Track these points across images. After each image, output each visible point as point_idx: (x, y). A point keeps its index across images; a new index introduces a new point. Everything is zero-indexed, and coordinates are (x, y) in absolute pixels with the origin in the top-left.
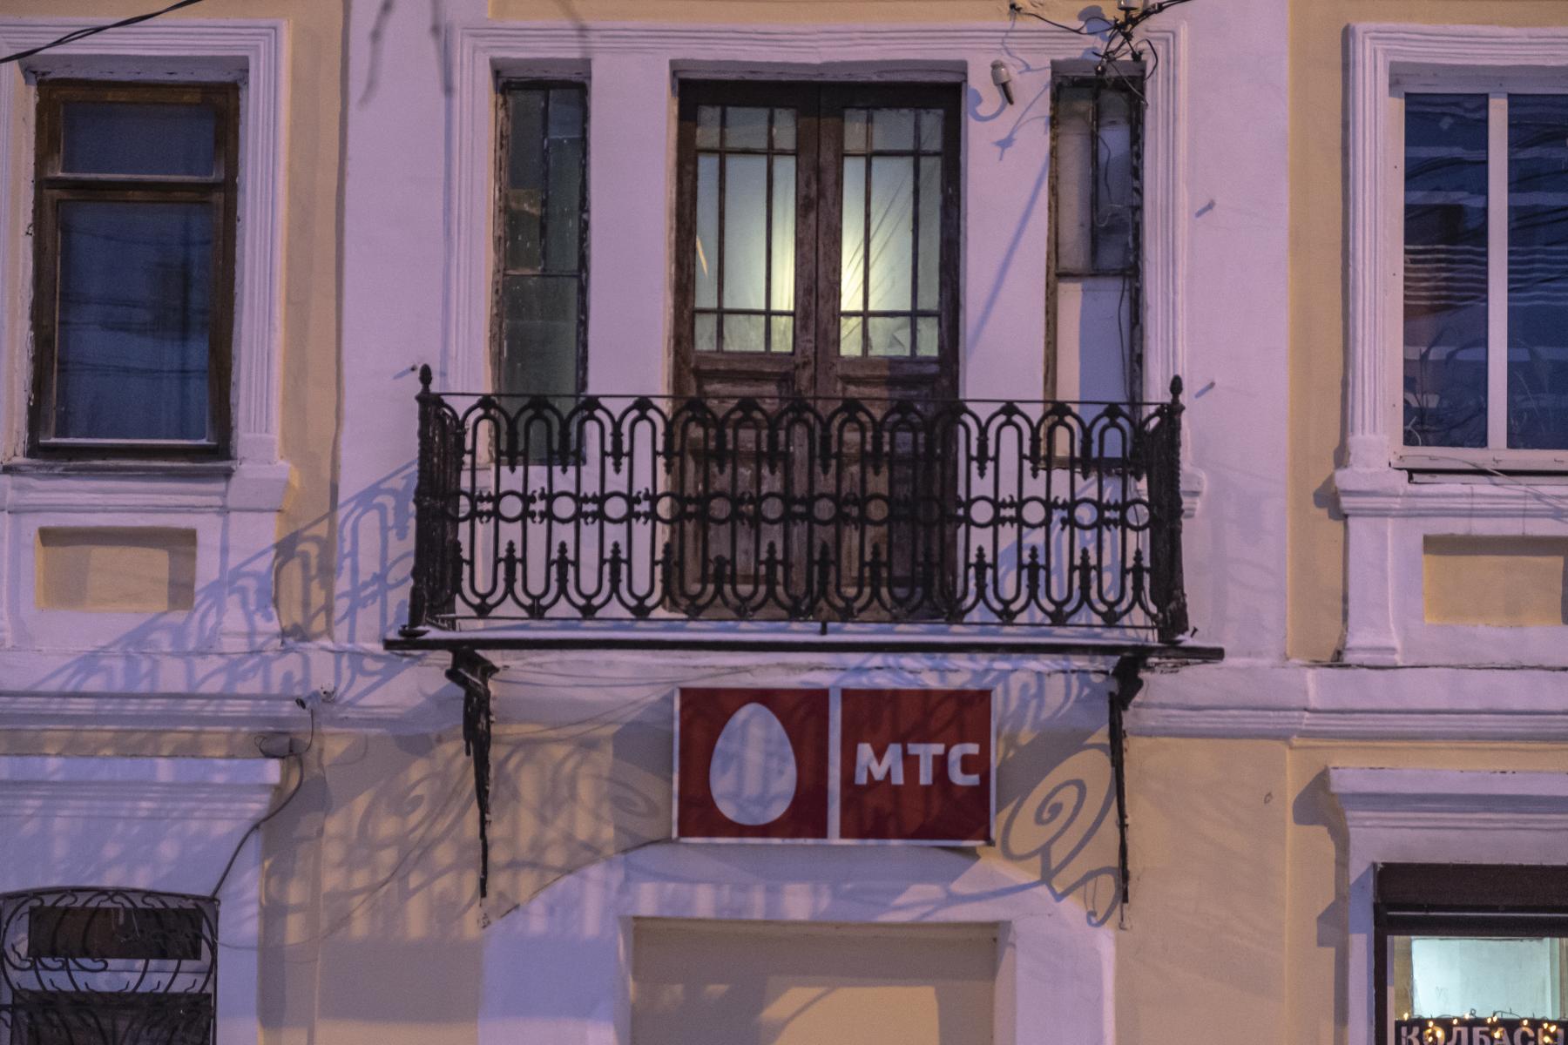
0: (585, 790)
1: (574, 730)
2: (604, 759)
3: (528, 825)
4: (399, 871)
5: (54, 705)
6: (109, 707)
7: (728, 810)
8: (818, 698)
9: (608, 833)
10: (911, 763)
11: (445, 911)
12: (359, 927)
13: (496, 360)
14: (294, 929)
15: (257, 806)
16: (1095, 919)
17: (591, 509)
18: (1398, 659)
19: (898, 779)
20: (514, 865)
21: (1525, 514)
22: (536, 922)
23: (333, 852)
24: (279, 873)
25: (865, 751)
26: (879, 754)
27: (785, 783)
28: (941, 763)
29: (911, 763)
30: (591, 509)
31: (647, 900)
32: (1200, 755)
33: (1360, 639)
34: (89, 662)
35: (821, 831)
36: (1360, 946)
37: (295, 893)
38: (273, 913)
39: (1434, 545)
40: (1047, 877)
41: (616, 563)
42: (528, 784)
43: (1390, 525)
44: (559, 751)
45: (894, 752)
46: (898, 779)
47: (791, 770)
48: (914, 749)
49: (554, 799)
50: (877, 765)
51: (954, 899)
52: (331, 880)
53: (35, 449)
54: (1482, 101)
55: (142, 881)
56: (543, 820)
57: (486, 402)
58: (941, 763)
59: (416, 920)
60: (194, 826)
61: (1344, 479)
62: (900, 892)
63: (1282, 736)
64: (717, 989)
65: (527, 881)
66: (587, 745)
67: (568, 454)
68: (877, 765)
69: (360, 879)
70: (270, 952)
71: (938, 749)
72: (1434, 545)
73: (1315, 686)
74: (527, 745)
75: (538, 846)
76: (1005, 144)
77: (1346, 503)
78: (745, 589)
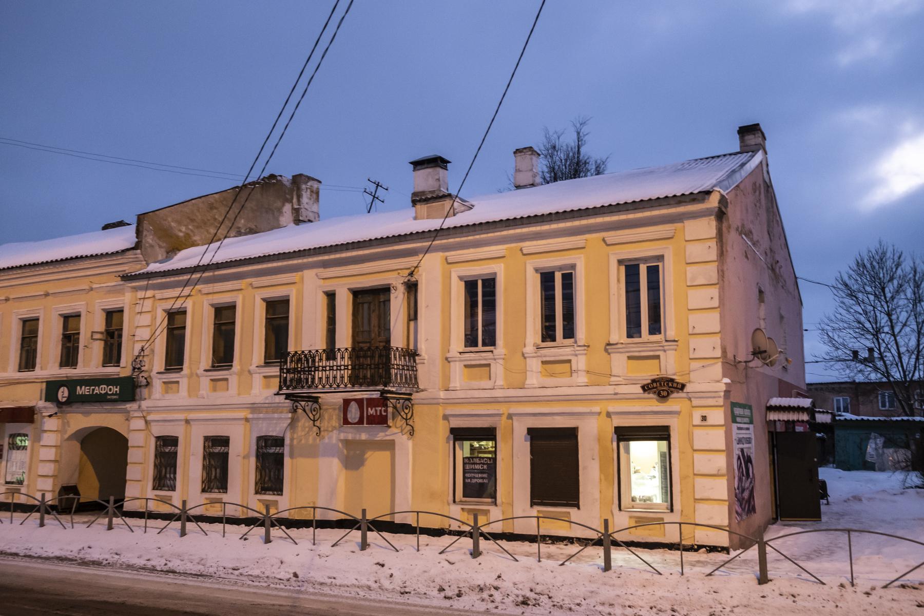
0: (334, 417)
1: (332, 407)
2: (337, 411)
3: (326, 423)
4: (308, 432)
5: (263, 405)
6: (270, 405)
7: (350, 420)
8: (362, 400)
9: (337, 425)
10: (376, 411)
11: (315, 440)
12: (303, 442)
13: (327, 343)
14: (295, 442)
15: (289, 421)
16: (409, 439)
17: (339, 368)
18: (458, 389)
19: (374, 414)
20: (324, 431)
21: (479, 360)
22: (326, 440)
23: (300, 429)
24: (293, 433)
25: (369, 409)
26: (372, 410)
27: (358, 415)
28: (381, 411)
29: (376, 411)
30: (339, 368)
31: (342, 436)
32: (426, 408)
33: (452, 385)
34: (266, 398)
35: (363, 424)
36: (452, 442)
37: (295, 436)
38: (292, 439)
39: (466, 366)
40: (402, 432)
41: (342, 377)
42: (326, 416)
43: (457, 363)
44: (331, 410)
45: (374, 409)
46: (374, 414)
47: (359, 413)
48: (377, 408)
49: (330, 419)
50: (371, 411)
51: (387, 435)
52: (300, 434)
53: (265, 363)
54: (476, 281)
55: (274, 434)
56: (329, 423)
57: (324, 350)
58: (381, 411)
59: (311, 441)
60: (282, 425)
61: (448, 355)
62: (378, 434)
63: (438, 404)
64: (358, 452)
65: (326, 433)
66: (334, 409)
67: (334, 359)
68: (371, 411)
69: (303, 433)
70: (291, 446)
71: (380, 408)
72: (466, 366)
73: (442, 394)
74: (327, 409)
75: (328, 427)
76: (396, 298)
77: (526, 355)
78: (361, 380)
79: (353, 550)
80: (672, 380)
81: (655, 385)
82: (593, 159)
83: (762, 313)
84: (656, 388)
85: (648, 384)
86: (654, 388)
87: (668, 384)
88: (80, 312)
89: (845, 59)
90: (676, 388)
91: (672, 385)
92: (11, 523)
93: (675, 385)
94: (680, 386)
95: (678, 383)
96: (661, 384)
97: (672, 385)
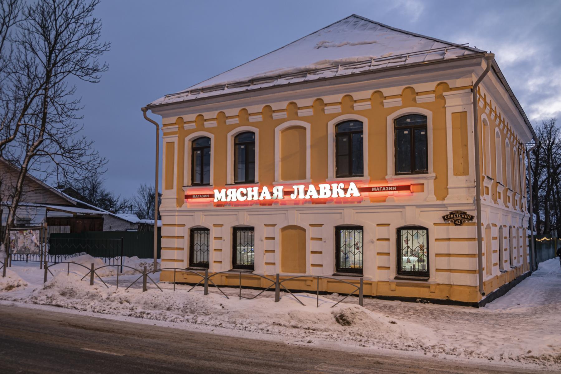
45: (223, 191)
79: (392, 325)
80: (464, 213)
81: (452, 216)
82: (101, 189)
83: (467, 222)
84: (453, 218)
85: (447, 216)
86: (451, 218)
87: (461, 216)
88: (378, 269)
89: (177, 135)
90: (467, 219)
91: (465, 216)
92: (379, 267)
93: (466, 216)
94: (470, 217)
95: (468, 215)
96: (456, 216)
97: (465, 216)
